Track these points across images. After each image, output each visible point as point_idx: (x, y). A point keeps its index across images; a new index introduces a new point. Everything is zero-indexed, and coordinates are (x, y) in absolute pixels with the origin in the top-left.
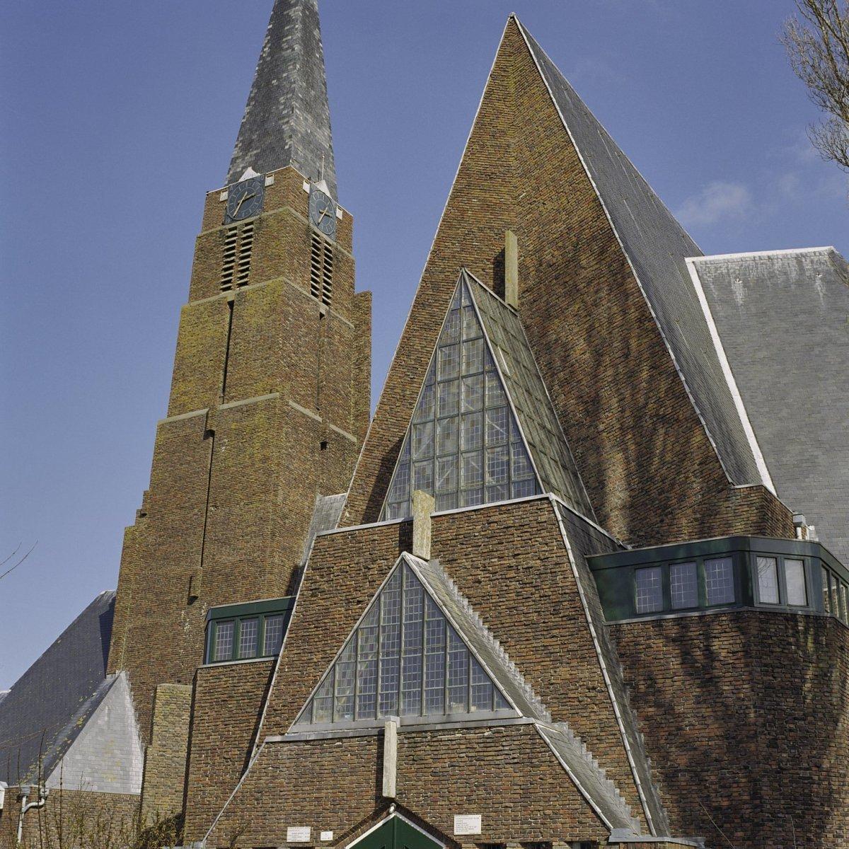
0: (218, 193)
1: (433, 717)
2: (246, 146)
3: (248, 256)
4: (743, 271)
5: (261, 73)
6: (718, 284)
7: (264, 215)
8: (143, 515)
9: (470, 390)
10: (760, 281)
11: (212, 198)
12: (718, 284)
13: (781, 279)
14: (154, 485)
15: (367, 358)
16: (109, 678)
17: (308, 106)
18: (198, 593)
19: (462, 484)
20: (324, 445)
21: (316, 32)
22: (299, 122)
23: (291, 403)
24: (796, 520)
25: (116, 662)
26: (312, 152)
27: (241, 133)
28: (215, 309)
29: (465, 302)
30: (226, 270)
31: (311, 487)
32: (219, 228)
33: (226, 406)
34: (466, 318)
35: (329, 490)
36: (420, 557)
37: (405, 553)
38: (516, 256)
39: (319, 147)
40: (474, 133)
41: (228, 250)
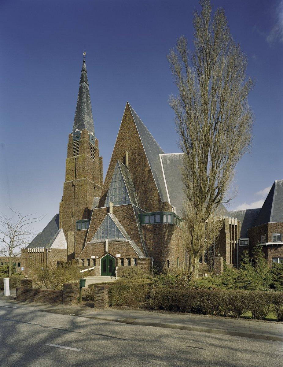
0: (71, 134)
1: (113, 240)
2: (76, 123)
3: (78, 149)
4: (169, 158)
5: (78, 105)
6: (165, 160)
7: (81, 140)
8: (63, 200)
9: (119, 183)
10: (172, 160)
11: (70, 135)
12: (165, 160)
13: (176, 159)
14: (64, 195)
15: (102, 170)
16: (59, 230)
17: (88, 114)
18: (74, 215)
19: (118, 200)
20: (95, 188)
21: (89, 95)
22: (87, 118)
23: (88, 180)
24: (172, 207)
25: (60, 227)
26: (89, 125)
27: (75, 120)
28: (72, 160)
29: (118, 167)
30: (74, 151)
31: (93, 196)
32: (72, 142)
33: (76, 180)
34: (118, 169)
35: (96, 196)
36: (111, 214)
37: (108, 213)
38: (128, 156)
39: (91, 124)
40: (120, 129)
41: (74, 147)
